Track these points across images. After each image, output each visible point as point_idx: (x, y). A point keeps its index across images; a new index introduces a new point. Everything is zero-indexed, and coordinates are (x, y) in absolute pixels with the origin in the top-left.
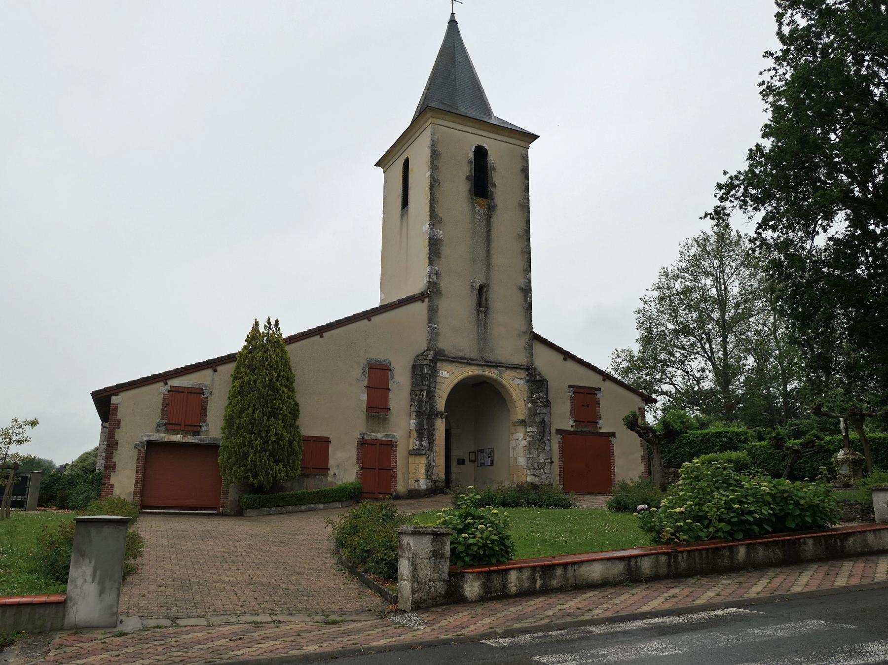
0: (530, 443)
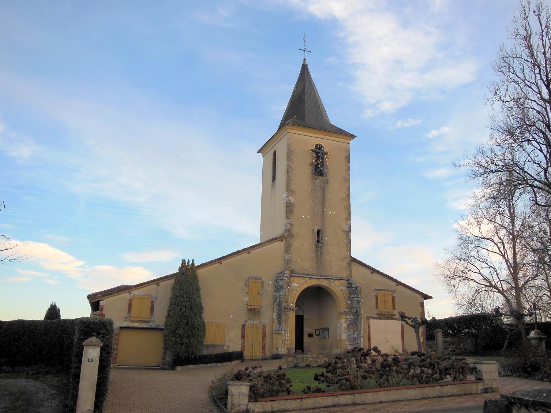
0: (349, 325)
